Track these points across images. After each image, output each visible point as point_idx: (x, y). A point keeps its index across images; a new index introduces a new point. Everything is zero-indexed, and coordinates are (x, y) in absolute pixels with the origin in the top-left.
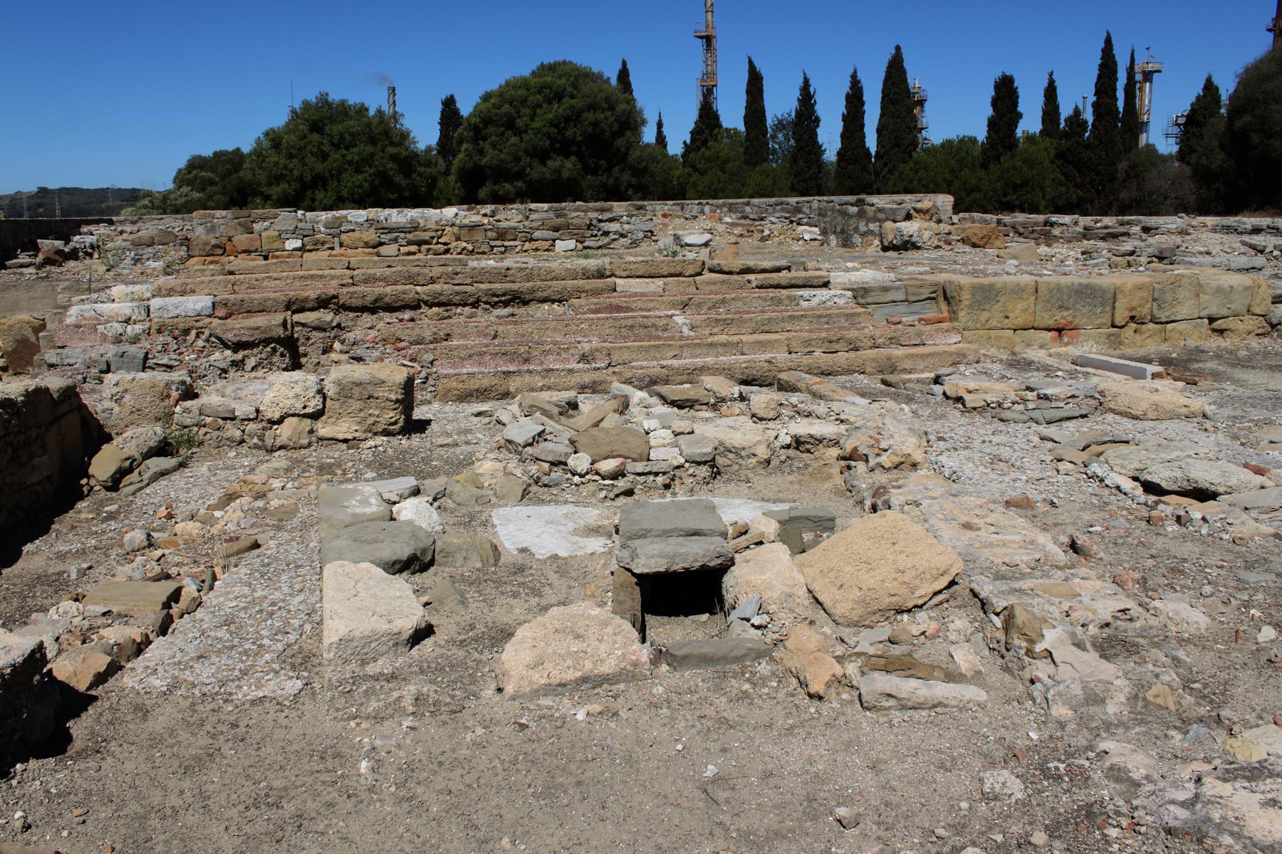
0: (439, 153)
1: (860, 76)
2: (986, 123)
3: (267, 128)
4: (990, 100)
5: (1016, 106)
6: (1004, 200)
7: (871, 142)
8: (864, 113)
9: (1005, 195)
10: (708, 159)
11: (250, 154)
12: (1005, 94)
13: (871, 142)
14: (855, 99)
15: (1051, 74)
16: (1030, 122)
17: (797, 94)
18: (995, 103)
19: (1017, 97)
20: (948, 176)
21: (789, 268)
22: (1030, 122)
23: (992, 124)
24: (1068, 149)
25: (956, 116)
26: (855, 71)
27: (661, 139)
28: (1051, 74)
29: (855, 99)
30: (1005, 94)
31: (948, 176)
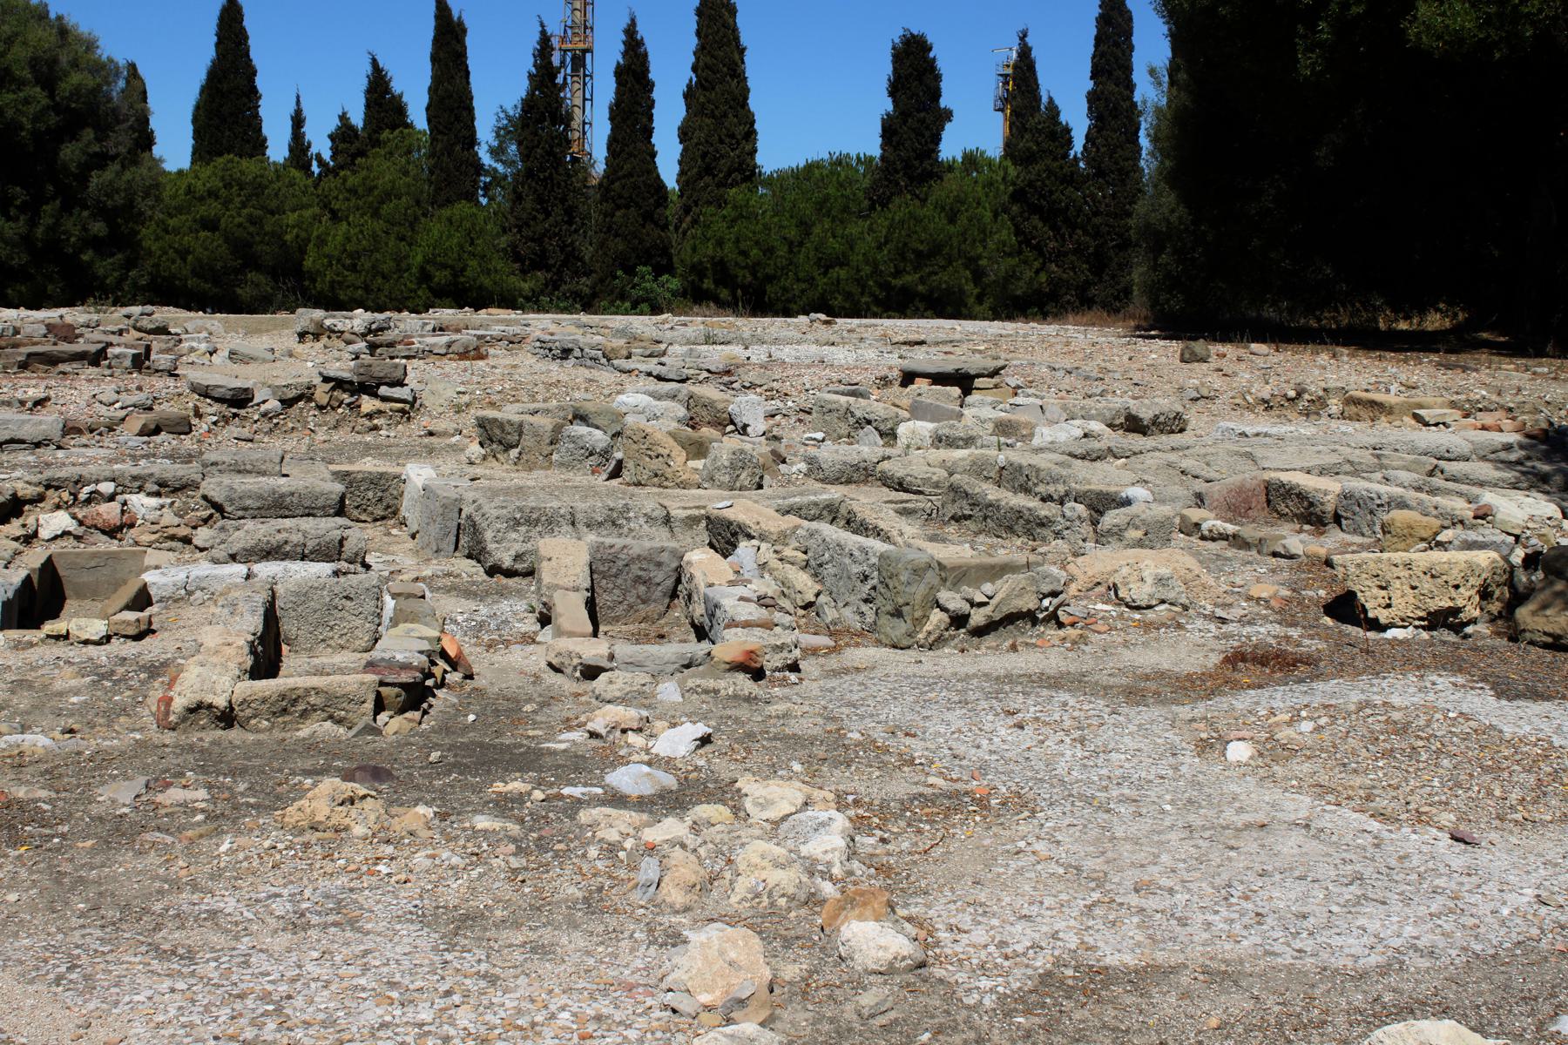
0: (601, 184)
1: (642, 31)
2: (879, 129)
3: (971, 147)
4: (885, 84)
5: (936, 94)
6: (898, 282)
7: (668, 168)
8: (652, 104)
9: (898, 273)
10: (353, 191)
11: (769, 182)
12: (914, 72)
13: (668, 168)
14: (634, 76)
15: (1023, 36)
16: (974, 129)
17: (528, 64)
18: (895, 90)
19: (938, 78)
20: (793, 233)
21: (1243, 434)
22: (974, 129)
23: (889, 131)
24: (1031, 184)
25: (818, 116)
26: (633, 23)
27: (299, 146)
28: (1023, 36)
29: (634, 76)
30: (914, 72)
31: (793, 233)
